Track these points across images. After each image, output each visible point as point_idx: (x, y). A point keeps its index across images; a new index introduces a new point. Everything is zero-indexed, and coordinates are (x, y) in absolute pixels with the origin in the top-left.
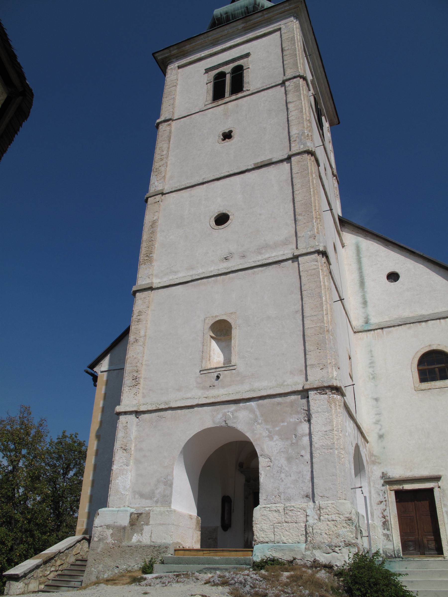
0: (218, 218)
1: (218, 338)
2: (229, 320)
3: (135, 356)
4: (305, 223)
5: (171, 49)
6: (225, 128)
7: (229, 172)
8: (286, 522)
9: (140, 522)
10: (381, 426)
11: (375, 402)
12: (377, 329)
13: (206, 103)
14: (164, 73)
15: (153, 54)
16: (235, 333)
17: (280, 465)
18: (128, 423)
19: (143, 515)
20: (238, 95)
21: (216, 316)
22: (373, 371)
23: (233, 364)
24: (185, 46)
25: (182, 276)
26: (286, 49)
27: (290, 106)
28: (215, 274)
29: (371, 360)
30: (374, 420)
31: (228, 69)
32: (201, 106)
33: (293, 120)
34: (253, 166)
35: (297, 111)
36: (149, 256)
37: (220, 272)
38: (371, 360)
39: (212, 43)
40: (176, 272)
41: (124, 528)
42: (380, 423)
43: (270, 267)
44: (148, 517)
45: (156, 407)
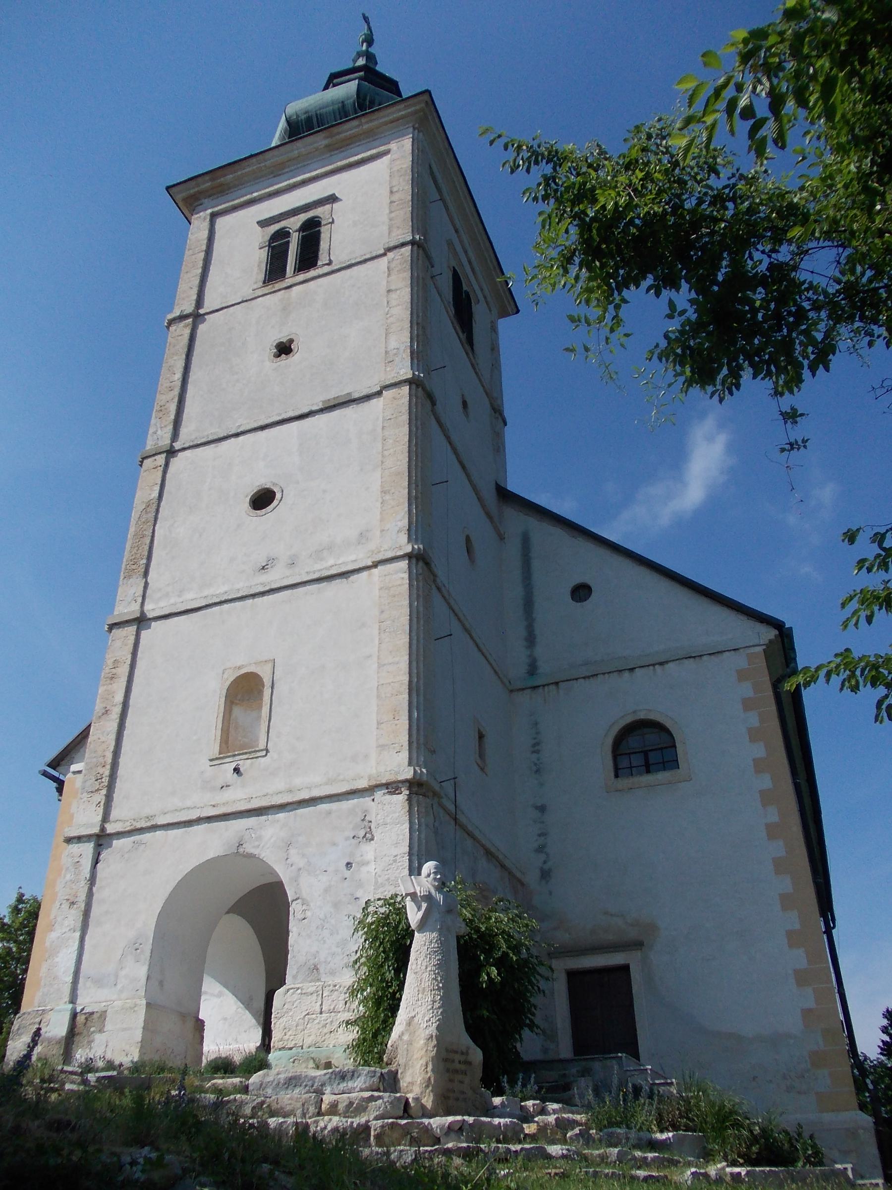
0: (260, 495)
3: (103, 739)
4: (393, 507)
5: (200, 179)
6: (282, 335)
7: (280, 414)
10: (547, 855)
13: (255, 286)
15: (168, 188)
17: (322, 916)
19: (95, 1016)
20: (307, 274)
22: (538, 760)
29: (535, 739)
31: (294, 223)
32: (247, 291)
33: (392, 324)
34: (321, 406)
35: (400, 307)
37: (252, 592)
38: (535, 739)
43: (301, 590)
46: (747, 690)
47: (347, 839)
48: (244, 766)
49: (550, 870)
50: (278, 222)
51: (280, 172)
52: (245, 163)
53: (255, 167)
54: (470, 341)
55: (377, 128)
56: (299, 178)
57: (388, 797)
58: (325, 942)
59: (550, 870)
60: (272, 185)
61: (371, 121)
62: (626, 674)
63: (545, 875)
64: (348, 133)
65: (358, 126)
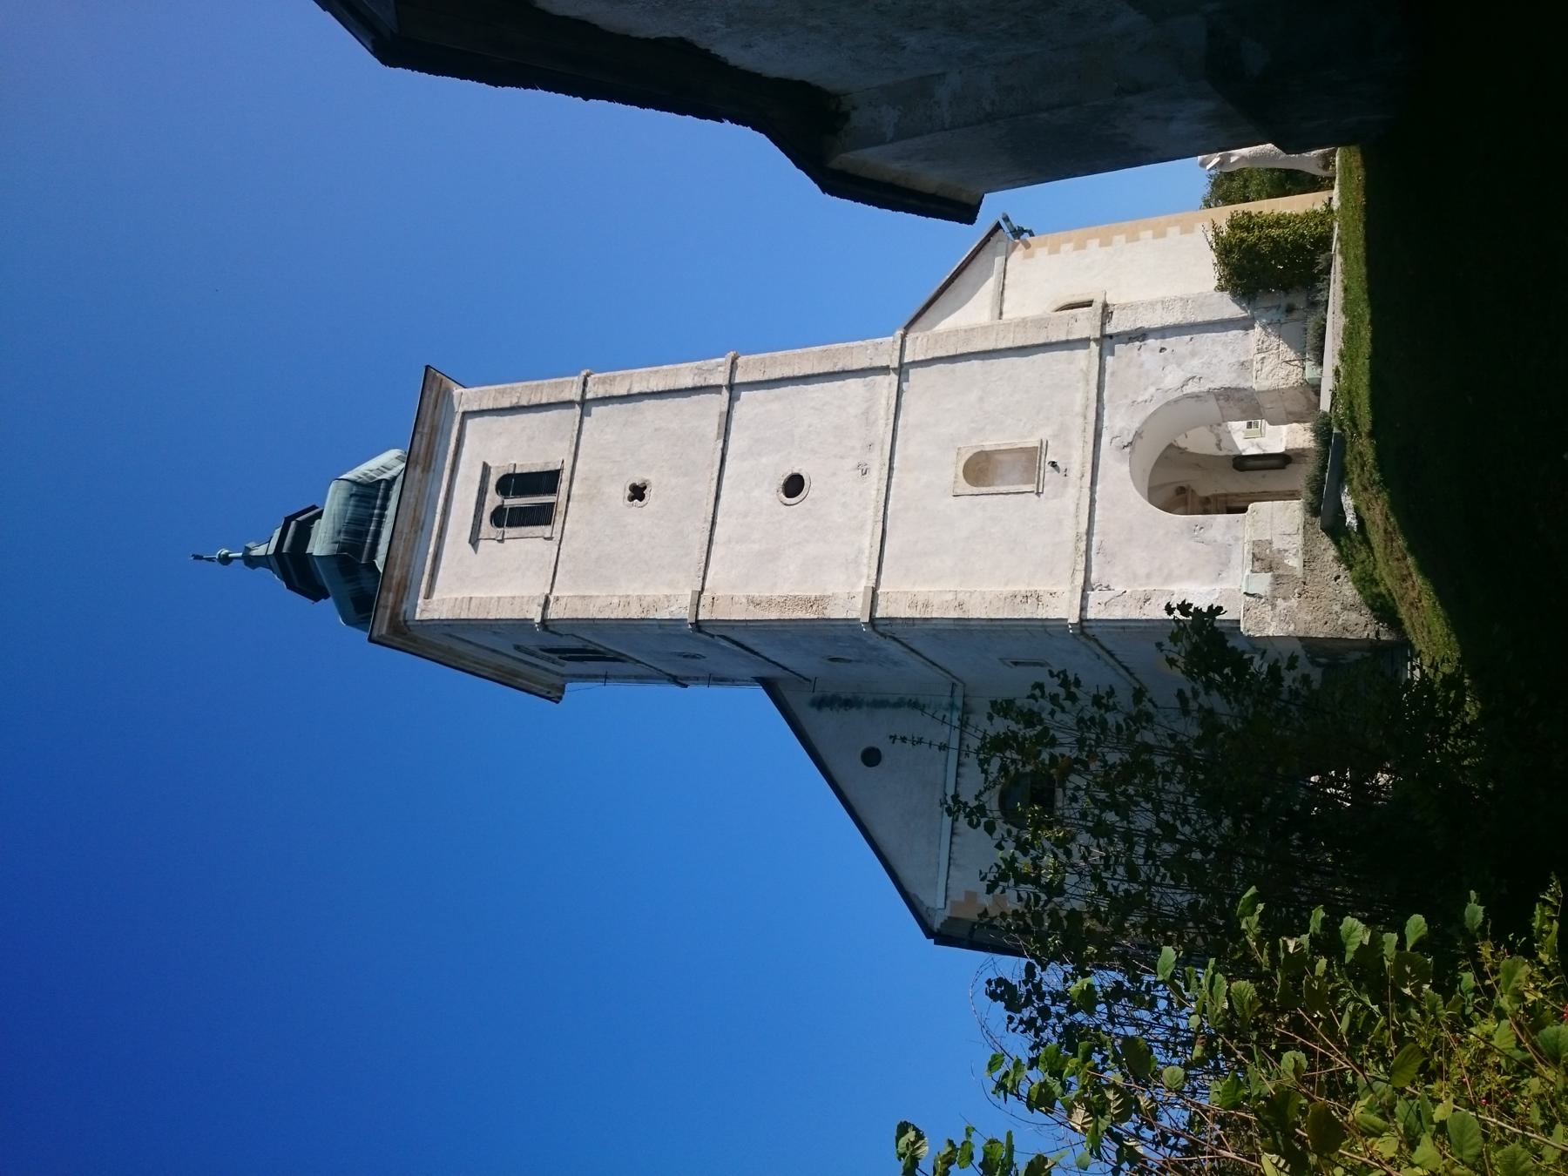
8: (1278, 348)
9: (1266, 555)
18: (1100, 601)
19: (1256, 551)
23: (1038, 445)
24: (392, 577)
25: (869, 542)
28: (885, 484)
36: (811, 603)
39: (416, 532)
40: (861, 551)
41: (1276, 578)
44: (1260, 543)
45: (1081, 556)
47: (1139, 355)
48: (1050, 458)
51: (421, 523)
53: (403, 544)
55: (433, 420)
56: (441, 501)
57: (1112, 322)
61: (424, 423)
65: (422, 436)
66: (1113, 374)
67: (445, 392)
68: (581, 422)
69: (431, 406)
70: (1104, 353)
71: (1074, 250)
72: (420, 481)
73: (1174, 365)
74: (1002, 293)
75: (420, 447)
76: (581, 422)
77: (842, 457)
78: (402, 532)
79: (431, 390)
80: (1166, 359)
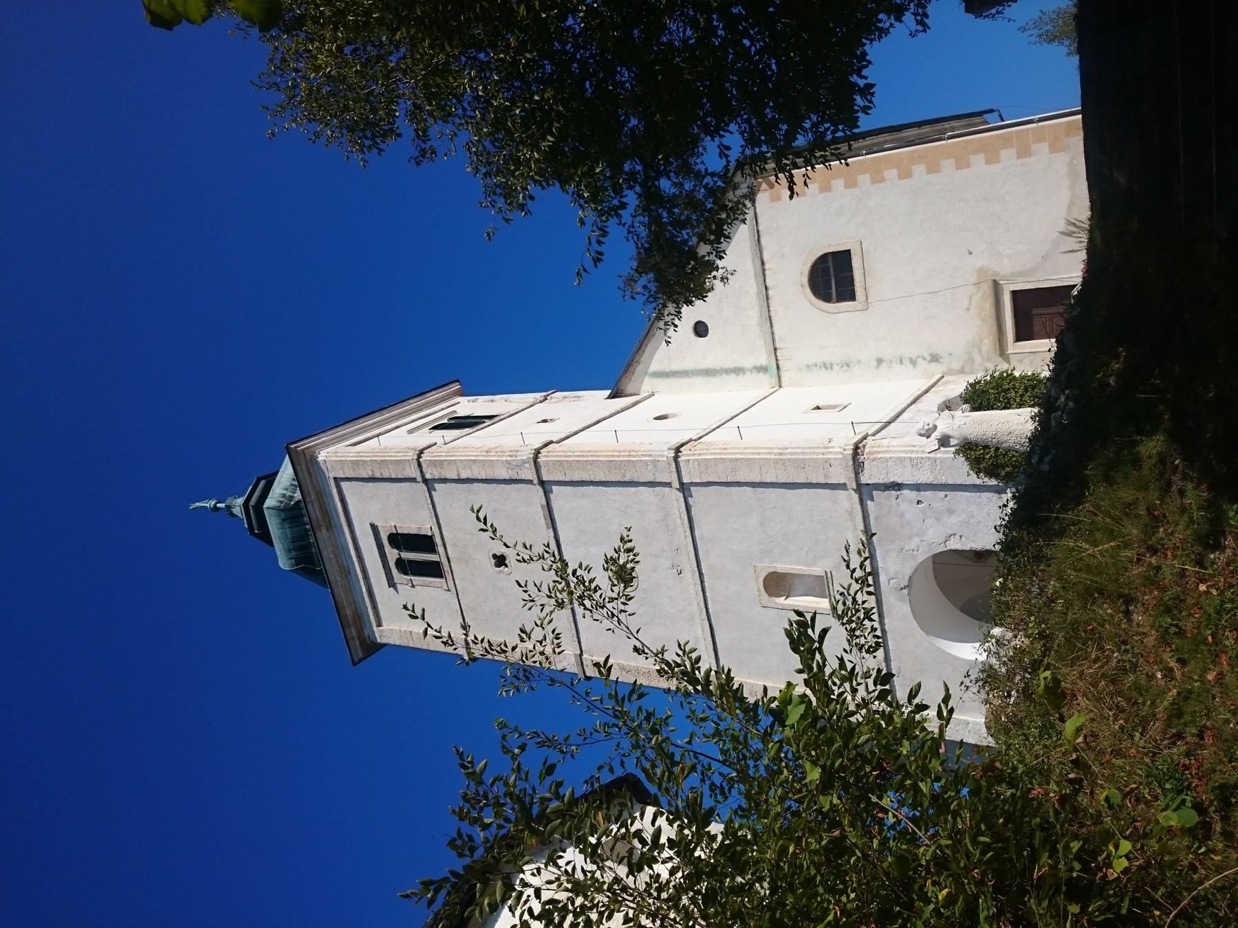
1: (787, 589)
2: (764, 574)
5: (348, 637)
10: (919, 357)
11: (884, 364)
12: (776, 356)
14: (385, 645)
15: (354, 664)
16: (782, 567)
20: (438, 544)
21: (759, 591)
26: (370, 473)
27: (464, 476)
28: (700, 589)
29: (820, 367)
30: (910, 366)
31: (392, 554)
38: (820, 367)
39: (346, 576)
42: (914, 358)
46: (1008, 154)
49: (931, 355)
50: (390, 570)
52: (338, 599)
54: (491, 417)
57: (865, 471)
58: (979, 522)
59: (931, 355)
60: (357, 576)
61: (309, 492)
62: (770, 292)
63: (935, 358)
64: (317, 511)
65: (313, 504)
66: (876, 519)
67: (311, 460)
68: (431, 497)
69: (307, 476)
70: (865, 497)
71: (820, 193)
72: (330, 538)
73: (933, 520)
74: (759, 240)
75: (315, 513)
76: (431, 497)
77: (656, 557)
78: (336, 581)
79: (300, 464)
80: (923, 512)
